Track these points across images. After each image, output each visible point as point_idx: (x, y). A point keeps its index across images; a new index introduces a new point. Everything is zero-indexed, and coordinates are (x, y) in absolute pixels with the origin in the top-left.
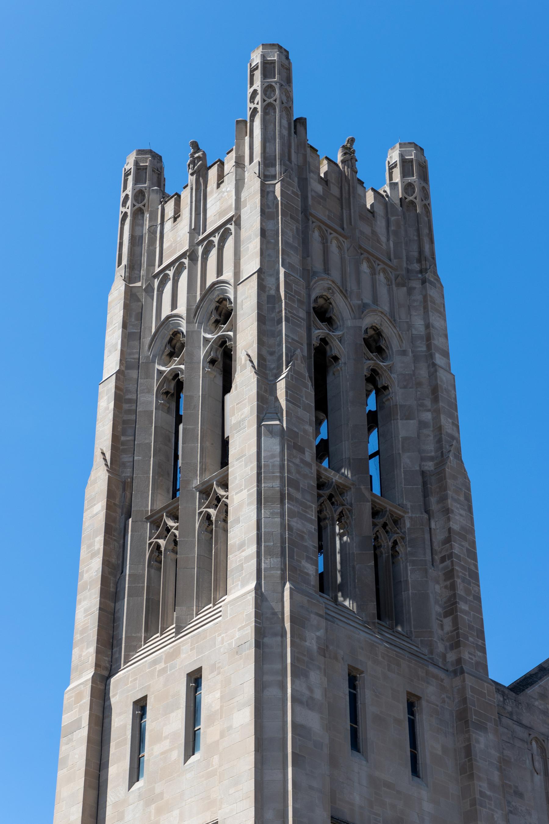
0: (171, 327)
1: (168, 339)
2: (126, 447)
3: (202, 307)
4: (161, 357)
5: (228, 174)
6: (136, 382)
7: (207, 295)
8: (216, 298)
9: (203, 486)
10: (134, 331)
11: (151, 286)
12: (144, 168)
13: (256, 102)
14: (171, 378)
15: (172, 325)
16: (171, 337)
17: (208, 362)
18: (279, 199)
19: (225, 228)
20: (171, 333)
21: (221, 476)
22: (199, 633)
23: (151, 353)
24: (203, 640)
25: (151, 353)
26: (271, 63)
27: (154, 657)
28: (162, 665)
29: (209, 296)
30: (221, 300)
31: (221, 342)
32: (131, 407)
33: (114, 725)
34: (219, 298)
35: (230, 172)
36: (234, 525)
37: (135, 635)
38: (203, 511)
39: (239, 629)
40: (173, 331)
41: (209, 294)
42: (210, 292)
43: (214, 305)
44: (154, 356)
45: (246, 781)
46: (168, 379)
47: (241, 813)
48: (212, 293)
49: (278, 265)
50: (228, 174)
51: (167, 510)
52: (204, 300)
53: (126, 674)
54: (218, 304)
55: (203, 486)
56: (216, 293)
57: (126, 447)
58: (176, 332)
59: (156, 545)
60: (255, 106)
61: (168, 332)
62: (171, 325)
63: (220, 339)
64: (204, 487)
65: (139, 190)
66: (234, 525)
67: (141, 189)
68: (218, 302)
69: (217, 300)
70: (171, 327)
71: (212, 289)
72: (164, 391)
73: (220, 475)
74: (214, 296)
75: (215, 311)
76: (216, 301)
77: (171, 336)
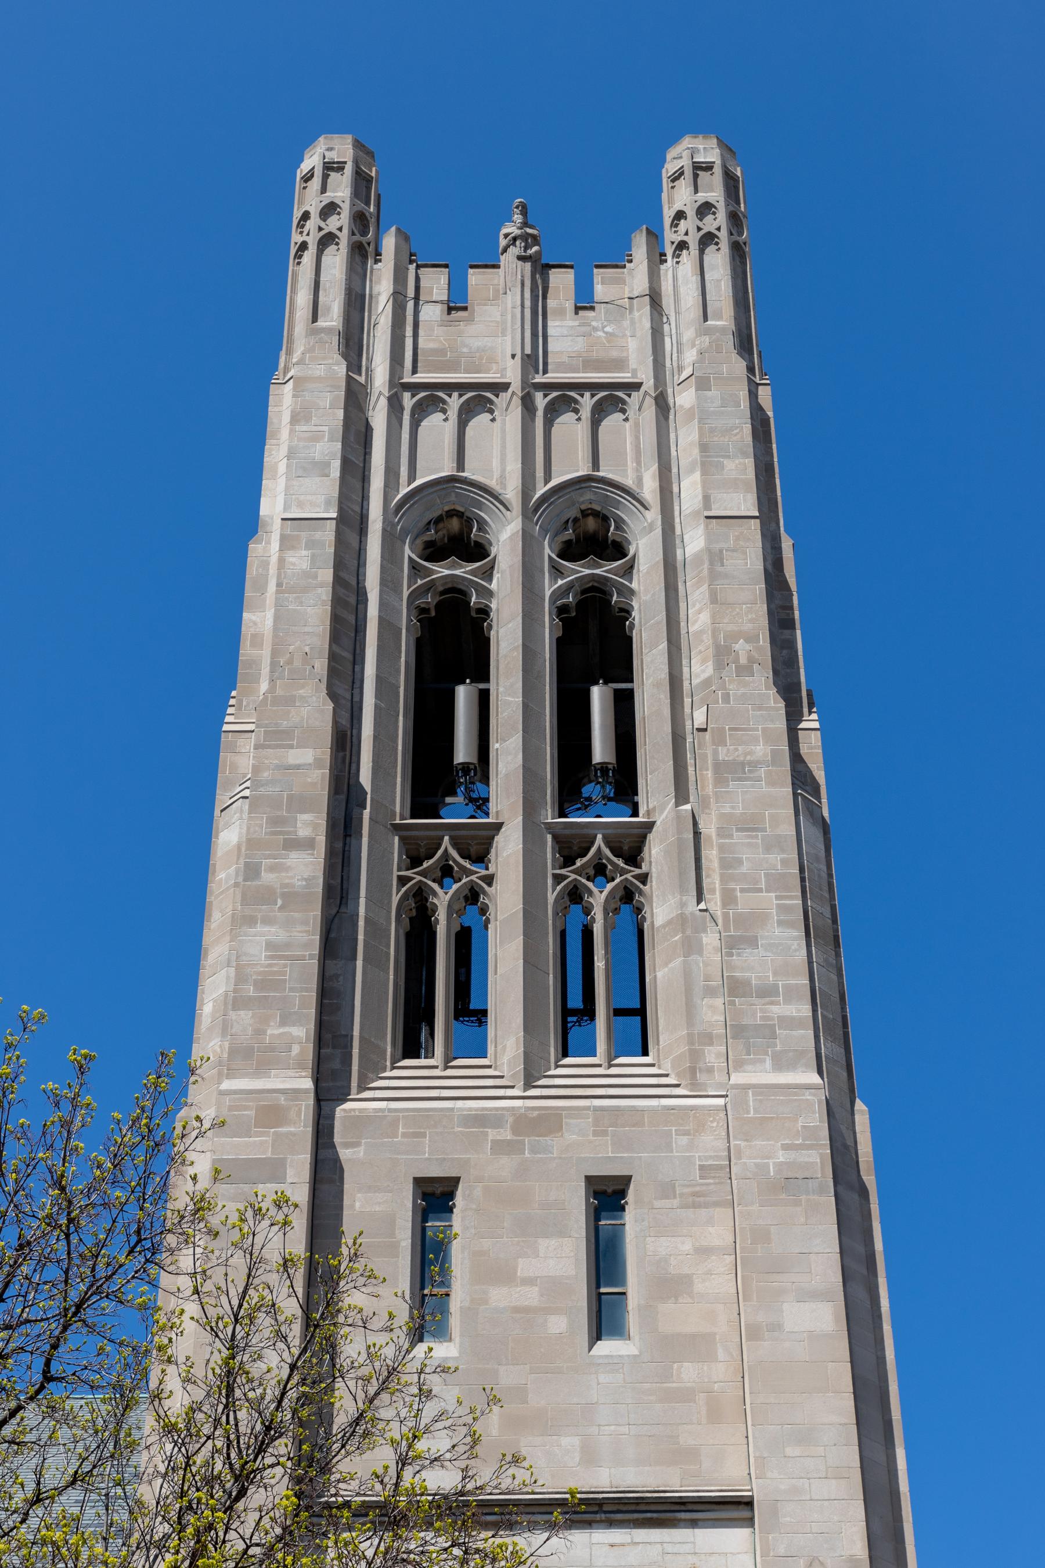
0: (453, 498)
4: (415, 539)
6: (356, 556)
7: (568, 490)
8: (583, 502)
9: (564, 829)
11: (663, 397)
13: (306, 230)
14: (441, 589)
18: (770, 414)
19: (611, 394)
20: (446, 508)
21: (619, 831)
22: (617, 1109)
23: (399, 521)
24: (634, 1126)
25: (399, 521)
27: (484, 1109)
28: (506, 1134)
29: (572, 494)
31: (590, 584)
33: (352, 1206)
34: (590, 506)
36: (742, 947)
37: (375, 1042)
38: (567, 877)
39: (786, 1148)
41: (573, 488)
44: (405, 532)
45: (835, 1445)
47: (826, 1503)
48: (580, 491)
49: (773, 525)
51: (453, 833)
52: (561, 494)
53: (386, 1113)
54: (579, 515)
55: (564, 829)
58: (455, 512)
59: (417, 888)
60: (305, 238)
62: (453, 495)
64: (567, 832)
66: (742, 947)
68: (582, 511)
69: (583, 507)
70: (453, 498)
71: (583, 485)
72: (423, 606)
73: (617, 828)
74: (582, 499)
77: (444, 513)
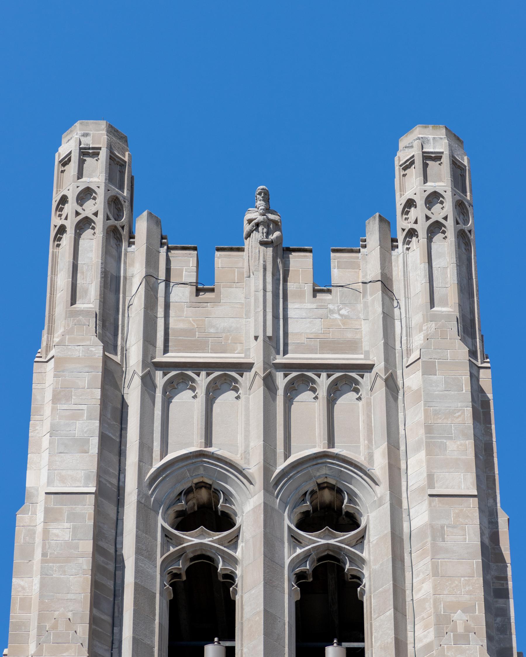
1: (186, 486)
2: (100, 630)
3: (291, 477)
5: (342, 286)
7: (307, 465)
8: (319, 477)
10: (110, 435)
12: (119, 162)
15: (204, 471)
16: (191, 487)
17: (295, 574)
18: (490, 396)
20: (196, 481)
26: (459, 166)
30: (325, 485)
31: (326, 553)
32: (107, 564)
34: (325, 480)
35: (350, 286)
40: (201, 480)
42: (314, 463)
43: (310, 486)
44: (158, 503)
46: (186, 556)
50: (342, 286)
52: (299, 470)
54: (316, 488)
56: (324, 471)
57: (100, 630)
58: (203, 484)
61: (192, 476)
62: (202, 468)
63: (328, 549)
65: (114, 196)
67: (118, 195)
68: (319, 485)
69: (320, 481)
70: (201, 471)
71: (320, 461)
72: (175, 571)
74: (318, 474)
75: (310, 497)
76: (317, 483)
77: (193, 485)
